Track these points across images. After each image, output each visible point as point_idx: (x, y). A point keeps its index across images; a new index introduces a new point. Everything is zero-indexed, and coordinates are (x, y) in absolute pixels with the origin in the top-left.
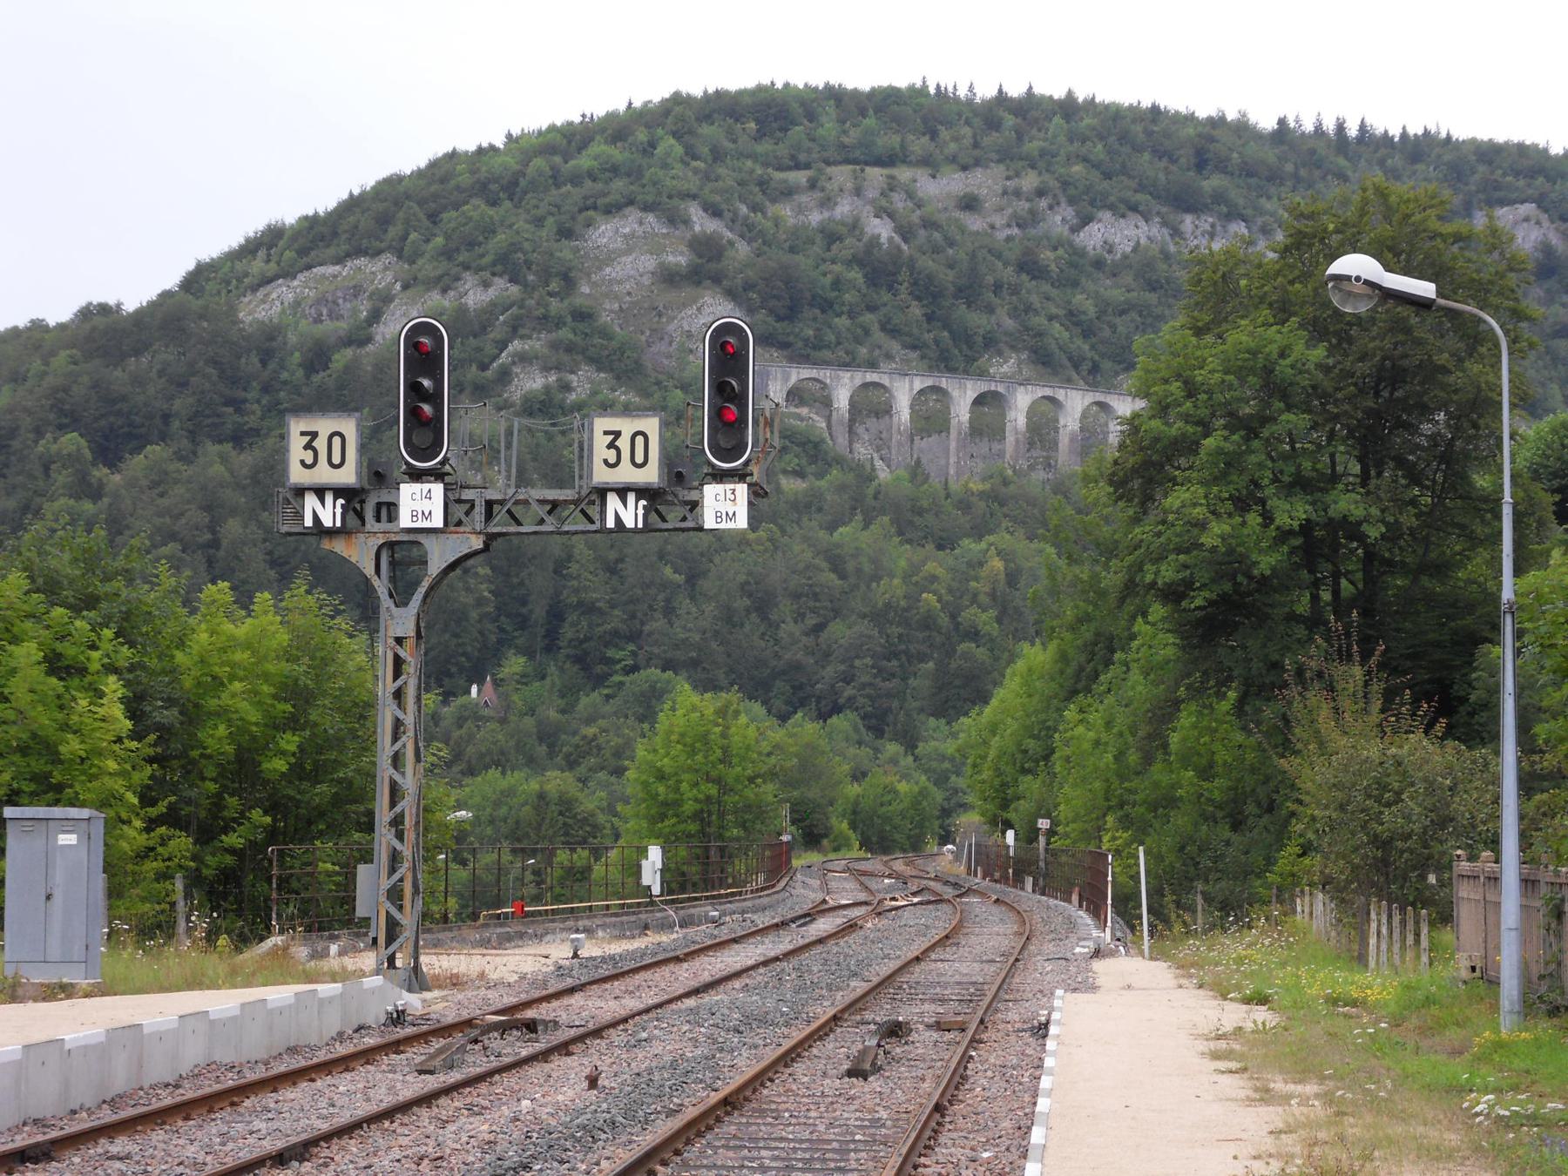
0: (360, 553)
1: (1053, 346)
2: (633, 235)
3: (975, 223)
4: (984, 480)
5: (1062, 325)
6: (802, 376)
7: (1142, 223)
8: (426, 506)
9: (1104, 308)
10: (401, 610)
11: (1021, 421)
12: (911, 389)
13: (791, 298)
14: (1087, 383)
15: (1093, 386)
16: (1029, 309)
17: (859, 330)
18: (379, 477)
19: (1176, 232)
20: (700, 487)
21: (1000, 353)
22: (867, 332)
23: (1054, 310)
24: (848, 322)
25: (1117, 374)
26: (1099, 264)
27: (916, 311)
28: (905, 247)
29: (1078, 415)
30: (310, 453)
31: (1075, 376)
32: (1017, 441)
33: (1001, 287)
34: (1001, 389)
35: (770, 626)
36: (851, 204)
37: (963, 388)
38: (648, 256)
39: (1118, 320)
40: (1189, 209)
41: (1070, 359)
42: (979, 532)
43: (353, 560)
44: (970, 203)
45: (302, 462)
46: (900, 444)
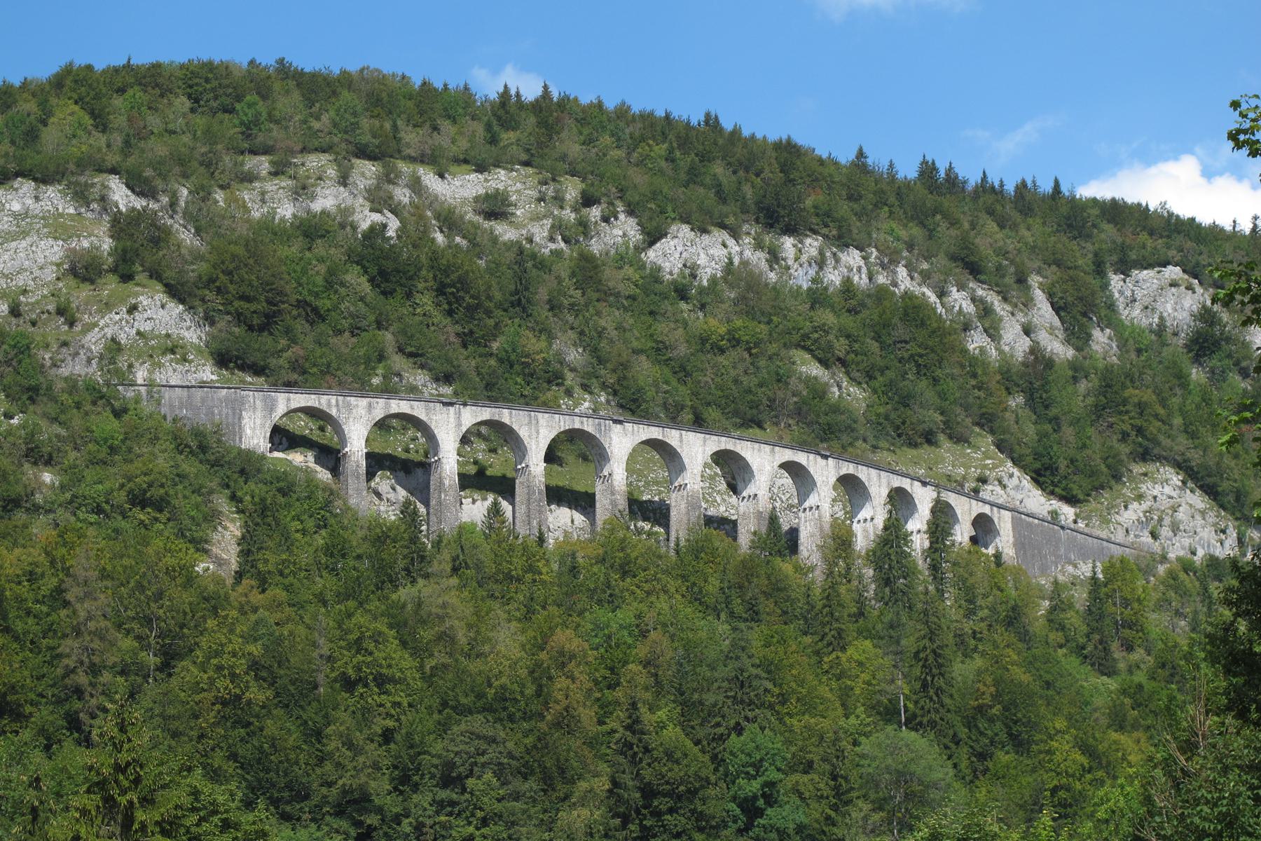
2: (26, 214)
3: (506, 233)
6: (294, 405)
7: (731, 242)
10: (974, 515)
12: (459, 425)
19: (774, 257)
26: (681, 292)
36: (336, 197)
40: (790, 230)
44: (495, 207)
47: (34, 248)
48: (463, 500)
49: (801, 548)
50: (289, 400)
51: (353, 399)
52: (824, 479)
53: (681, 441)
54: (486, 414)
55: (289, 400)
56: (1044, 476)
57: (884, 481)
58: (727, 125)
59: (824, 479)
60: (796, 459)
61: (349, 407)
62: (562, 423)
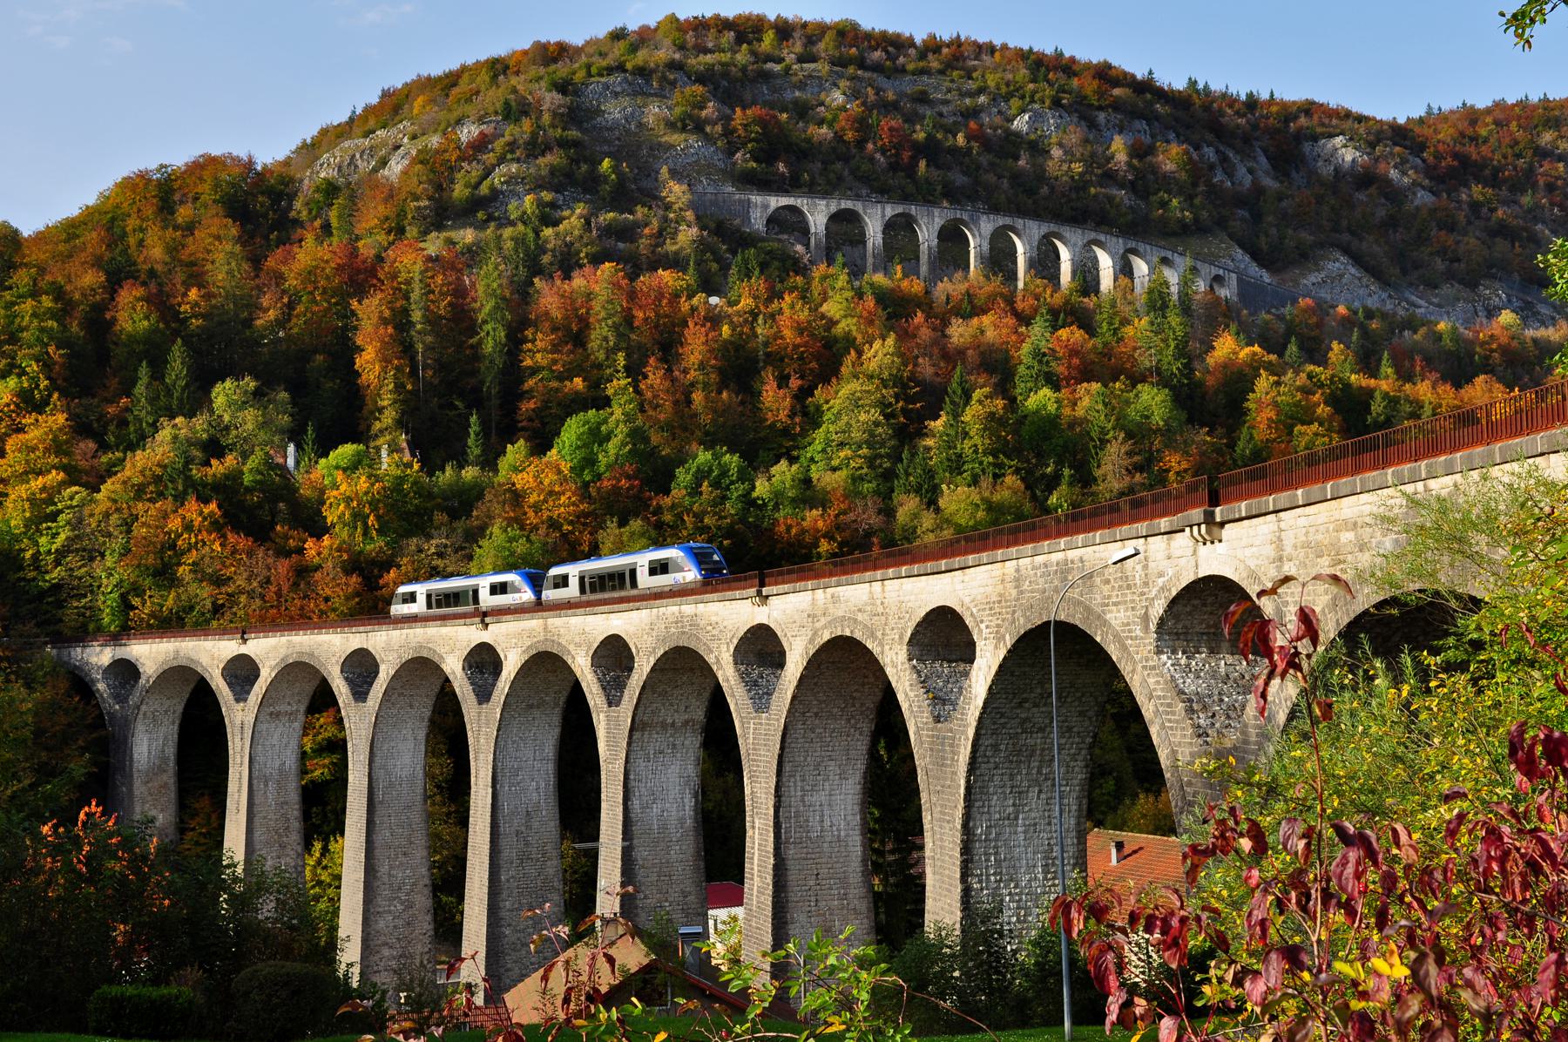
12: (883, 216)
37: (931, 215)
54: (899, 209)
56: (1256, 255)
58: (1067, 54)
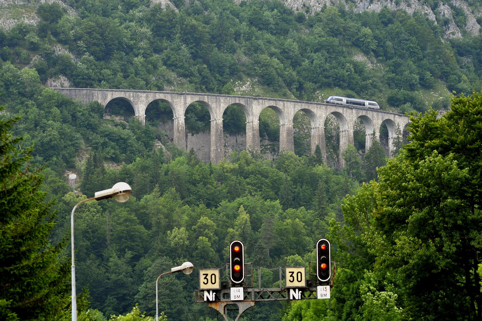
0: (220, 308)
1: (274, 72)
4: (233, 162)
5: (279, 59)
8: (238, 294)
9: (304, 47)
11: (256, 123)
12: (185, 103)
13: (106, 45)
14: (295, 97)
15: (300, 98)
16: (257, 49)
17: (150, 66)
18: (225, 286)
20: (316, 287)
21: (240, 79)
22: (155, 67)
23: (273, 50)
24: (142, 60)
25: (314, 90)
26: (300, 19)
27: (184, 49)
28: (177, 11)
29: (291, 118)
30: (206, 280)
31: (289, 93)
32: (254, 135)
33: (240, 35)
34: (242, 102)
35: (103, 260)
38: (12, 20)
39: (315, 56)
41: (285, 81)
42: (233, 195)
43: (218, 310)
45: (204, 283)
46: (179, 138)
47: (4, 24)
48: (188, 134)
49: (341, 149)
50: (112, 94)
51: (140, 93)
52: (351, 118)
53: (284, 106)
55: (112, 94)
57: (380, 117)
59: (351, 118)
60: (337, 111)
61: (138, 97)
62: (231, 101)
